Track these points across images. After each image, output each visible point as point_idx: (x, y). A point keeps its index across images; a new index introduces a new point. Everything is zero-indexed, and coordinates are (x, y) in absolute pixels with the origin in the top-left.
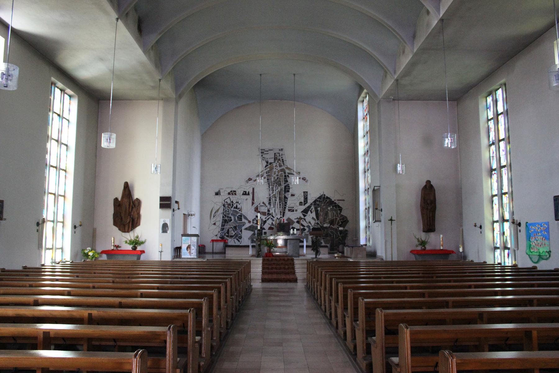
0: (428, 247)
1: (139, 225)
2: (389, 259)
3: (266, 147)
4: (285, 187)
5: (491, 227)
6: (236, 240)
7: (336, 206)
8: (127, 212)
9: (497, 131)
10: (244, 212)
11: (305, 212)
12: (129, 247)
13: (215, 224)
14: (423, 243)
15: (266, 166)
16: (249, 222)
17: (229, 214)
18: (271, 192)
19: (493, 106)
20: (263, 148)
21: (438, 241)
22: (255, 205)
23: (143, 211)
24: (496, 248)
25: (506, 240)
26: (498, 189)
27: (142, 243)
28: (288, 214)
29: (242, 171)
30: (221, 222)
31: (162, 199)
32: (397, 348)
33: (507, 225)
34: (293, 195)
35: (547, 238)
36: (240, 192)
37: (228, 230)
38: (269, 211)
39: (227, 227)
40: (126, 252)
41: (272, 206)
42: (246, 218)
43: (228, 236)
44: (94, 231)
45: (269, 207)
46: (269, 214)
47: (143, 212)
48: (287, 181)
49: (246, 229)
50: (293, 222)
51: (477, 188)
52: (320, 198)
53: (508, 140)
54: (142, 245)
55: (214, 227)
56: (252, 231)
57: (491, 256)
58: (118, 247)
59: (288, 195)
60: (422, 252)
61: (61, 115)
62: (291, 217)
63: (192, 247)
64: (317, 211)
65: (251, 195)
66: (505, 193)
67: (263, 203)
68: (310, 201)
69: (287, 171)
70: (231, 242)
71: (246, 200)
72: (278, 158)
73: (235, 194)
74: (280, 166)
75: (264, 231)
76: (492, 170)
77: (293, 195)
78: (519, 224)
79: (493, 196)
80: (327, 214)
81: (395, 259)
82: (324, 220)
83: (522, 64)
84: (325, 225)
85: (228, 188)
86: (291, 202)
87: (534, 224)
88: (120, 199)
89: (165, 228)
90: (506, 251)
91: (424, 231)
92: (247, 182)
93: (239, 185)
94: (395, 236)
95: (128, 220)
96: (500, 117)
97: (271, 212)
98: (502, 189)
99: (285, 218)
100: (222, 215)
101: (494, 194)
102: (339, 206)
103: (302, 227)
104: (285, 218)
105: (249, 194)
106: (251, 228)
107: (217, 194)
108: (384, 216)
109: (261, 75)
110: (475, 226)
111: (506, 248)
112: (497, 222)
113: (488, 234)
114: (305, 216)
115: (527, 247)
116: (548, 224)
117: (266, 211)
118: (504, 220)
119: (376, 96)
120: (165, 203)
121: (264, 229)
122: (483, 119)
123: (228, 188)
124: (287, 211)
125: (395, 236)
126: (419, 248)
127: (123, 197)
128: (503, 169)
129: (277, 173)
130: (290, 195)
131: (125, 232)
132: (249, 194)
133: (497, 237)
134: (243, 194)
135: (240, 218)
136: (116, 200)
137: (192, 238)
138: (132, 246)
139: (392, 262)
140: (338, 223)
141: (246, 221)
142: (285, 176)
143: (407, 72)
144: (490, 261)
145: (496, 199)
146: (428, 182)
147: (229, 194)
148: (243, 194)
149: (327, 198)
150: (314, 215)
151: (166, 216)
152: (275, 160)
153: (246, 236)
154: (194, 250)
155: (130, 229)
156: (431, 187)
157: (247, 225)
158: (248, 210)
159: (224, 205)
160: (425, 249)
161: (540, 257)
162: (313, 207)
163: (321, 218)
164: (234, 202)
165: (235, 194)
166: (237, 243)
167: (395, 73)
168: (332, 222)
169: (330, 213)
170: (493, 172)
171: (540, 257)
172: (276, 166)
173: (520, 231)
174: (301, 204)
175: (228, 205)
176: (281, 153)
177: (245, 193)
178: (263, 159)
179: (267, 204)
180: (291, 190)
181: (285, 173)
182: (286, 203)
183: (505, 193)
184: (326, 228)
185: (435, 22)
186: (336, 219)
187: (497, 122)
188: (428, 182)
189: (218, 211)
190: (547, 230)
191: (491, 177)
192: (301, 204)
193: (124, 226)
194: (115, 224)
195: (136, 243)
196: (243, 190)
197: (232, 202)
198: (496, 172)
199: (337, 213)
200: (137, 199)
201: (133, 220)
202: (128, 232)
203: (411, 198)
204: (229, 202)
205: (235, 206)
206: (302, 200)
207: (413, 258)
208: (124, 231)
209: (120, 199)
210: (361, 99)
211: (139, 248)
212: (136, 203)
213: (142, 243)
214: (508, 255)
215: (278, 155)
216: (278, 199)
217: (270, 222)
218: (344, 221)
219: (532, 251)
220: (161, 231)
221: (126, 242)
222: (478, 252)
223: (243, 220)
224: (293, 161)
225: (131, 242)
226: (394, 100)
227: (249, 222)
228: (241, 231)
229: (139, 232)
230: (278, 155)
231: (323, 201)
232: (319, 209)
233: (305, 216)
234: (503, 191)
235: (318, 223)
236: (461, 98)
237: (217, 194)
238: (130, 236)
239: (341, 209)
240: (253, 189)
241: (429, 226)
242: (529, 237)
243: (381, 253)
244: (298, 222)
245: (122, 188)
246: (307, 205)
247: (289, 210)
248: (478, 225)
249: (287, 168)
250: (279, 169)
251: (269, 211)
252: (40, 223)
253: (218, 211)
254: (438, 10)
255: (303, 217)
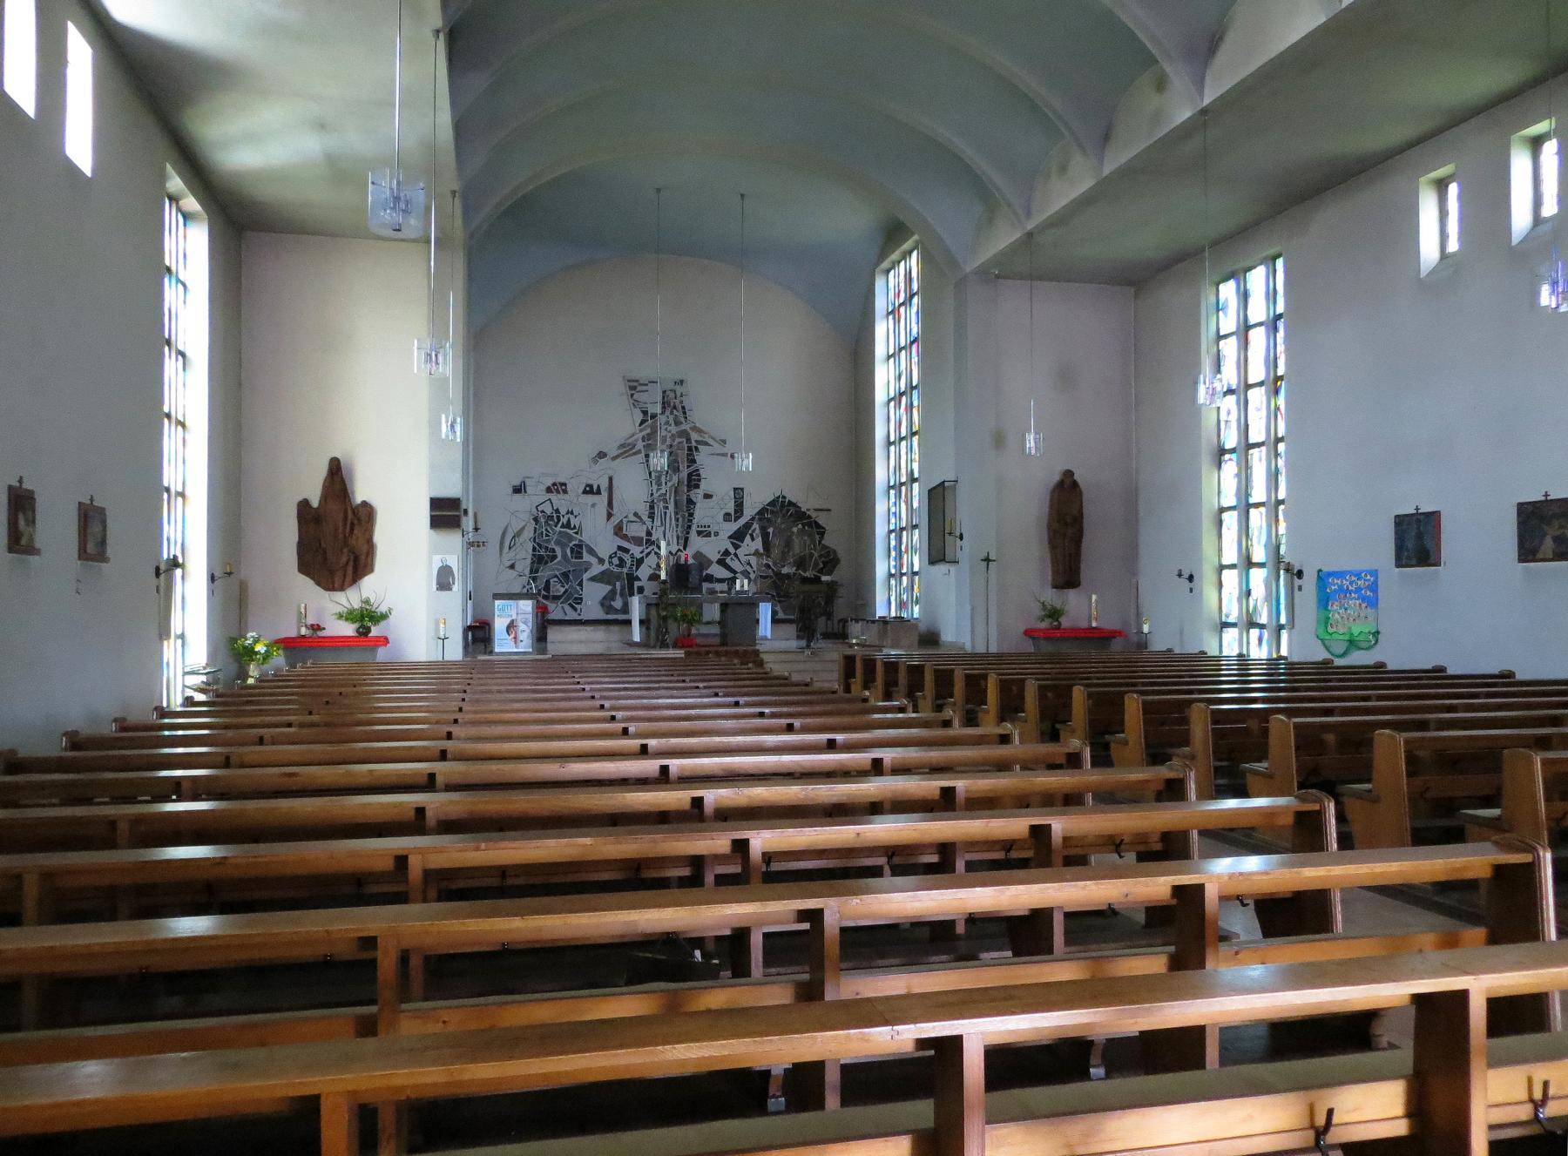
0: (1065, 622)
1: (372, 571)
2: (981, 649)
3: (643, 374)
4: (690, 475)
5: (1214, 578)
6: (567, 608)
7: (810, 524)
8: (336, 537)
9: (1243, 364)
10: (585, 537)
11: (738, 537)
12: (348, 630)
13: (512, 567)
14: (1054, 614)
15: (643, 422)
16: (601, 561)
17: (548, 541)
18: (655, 487)
19: (1245, 309)
20: (634, 375)
21: (1085, 607)
22: (615, 521)
23: (383, 535)
24: (1225, 625)
25: (1255, 607)
26: (1238, 494)
27: (384, 617)
28: (697, 543)
29: (580, 435)
30: (529, 561)
31: (436, 503)
32: (1352, 848)
33: (1258, 577)
34: (708, 496)
35: (1373, 603)
36: (576, 487)
37: (548, 582)
38: (649, 533)
39: (545, 573)
40: (340, 643)
41: (657, 522)
42: (592, 552)
43: (545, 597)
44: (243, 588)
45: (649, 524)
46: (650, 542)
47: (380, 535)
48: (694, 461)
49: (593, 579)
50: (710, 563)
51: (1185, 490)
52: (772, 503)
53: (1273, 384)
54: (383, 623)
55: (513, 573)
56: (608, 583)
57: (1215, 644)
58: (316, 628)
59: (697, 495)
60: (1051, 630)
61: (174, 268)
62: (704, 551)
63: (522, 627)
64: (765, 536)
65: (605, 494)
66: (1257, 505)
67: (636, 514)
68: (749, 511)
69: (694, 436)
70: (556, 611)
71: (593, 505)
72: (673, 404)
73: (565, 492)
74: (677, 423)
75: (637, 584)
76: (1222, 451)
77: (708, 496)
78: (1300, 574)
79: (1222, 510)
80: (788, 544)
81: (993, 649)
82: (784, 559)
83: (1329, 218)
84: (785, 570)
85: (547, 475)
86: (704, 513)
87: (1340, 575)
88: (315, 503)
89: (444, 580)
90: (1254, 633)
91: (1055, 587)
92: (596, 462)
93: (573, 465)
94: (993, 597)
95: (344, 559)
96: (1252, 333)
97: (654, 538)
98: (1248, 495)
99: (690, 551)
100: (530, 546)
101: (1225, 504)
102: (818, 526)
103: (729, 575)
104: (690, 551)
105: (599, 492)
106: (602, 578)
107: (518, 490)
108: (966, 551)
109: (659, 190)
110: (1180, 575)
111: (1252, 624)
112: (1233, 566)
113: (1210, 594)
114: (736, 547)
115: (1318, 622)
116: (1375, 573)
117: (643, 534)
118: (1248, 563)
119: (953, 264)
120: (445, 514)
121: (638, 579)
122: (1207, 334)
123: (547, 475)
124: (693, 534)
125: (993, 597)
126: (1044, 625)
127: (325, 497)
128: (1254, 452)
129: (669, 441)
130: (700, 497)
131: (333, 589)
132: (599, 492)
133: (1230, 601)
134: (585, 492)
135: (577, 551)
136: (304, 506)
137: (522, 602)
138: (356, 625)
139: (986, 655)
140: (816, 563)
141: (594, 560)
142: (690, 449)
143: (1061, 219)
144: (1212, 651)
145: (1231, 519)
146: (1069, 474)
147: (549, 490)
148: (585, 492)
149: (790, 503)
150: (758, 544)
151: (450, 549)
152: (664, 408)
153: (593, 594)
154: (525, 631)
155: (349, 578)
156: (1075, 484)
157: (597, 569)
158: (599, 536)
159: (536, 520)
160: (1058, 628)
161: (1352, 644)
162: (756, 526)
163: (776, 552)
164: (563, 511)
165: (565, 492)
166: (571, 615)
167: (1029, 214)
168: (801, 563)
169: (796, 542)
170: (1227, 457)
171: (1352, 644)
172: (667, 423)
173: (1300, 588)
174: (727, 517)
175: (546, 520)
176: (679, 389)
177: (590, 490)
178: (636, 403)
179: (645, 518)
180: (703, 484)
181: (689, 440)
182: (691, 515)
183: (1257, 505)
184: (788, 576)
185: (1183, 114)
186: (811, 555)
187: (1244, 344)
188: (1069, 474)
189: (518, 534)
190: (1374, 587)
191: (1219, 467)
192: (727, 517)
193: (332, 573)
194: (304, 568)
195: (367, 617)
196: (584, 481)
197: (557, 511)
198: (1234, 456)
199: (813, 541)
200: (365, 504)
201: (356, 559)
202: (342, 589)
203: (1028, 510)
204: (549, 511)
205: (564, 520)
206: (731, 508)
207: (1028, 647)
208: (330, 587)
209: (315, 503)
210: (885, 265)
211: (375, 631)
212: (363, 513)
213: (384, 617)
214: (1260, 640)
215: (672, 395)
216: (671, 506)
217: (651, 561)
218: (830, 561)
219: (1330, 630)
220: (435, 587)
221: (340, 616)
222: (1181, 633)
223: (586, 557)
224: (705, 412)
225: (349, 616)
226: (997, 277)
227: (601, 561)
228: (581, 584)
229: (371, 588)
230: (672, 395)
231: (781, 510)
232: (771, 530)
233: (736, 547)
234: (1252, 501)
235: (768, 566)
236: (1150, 288)
237: (518, 490)
238: (350, 599)
239: (822, 532)
240: (611, 479)
241: (1067, 574)
242: (1324, 601)
243: (949, 635)
244: (721, 562)
245: (322, 471)
246: (742, 521)
247: (699, 533)
248: (1186, 574)
249: (695, 429)
250: (674, 429)
251: (649, 533)
252: (163, 567)
253: (518, 534)
254: (1199, 84)
255: (732, 550)
